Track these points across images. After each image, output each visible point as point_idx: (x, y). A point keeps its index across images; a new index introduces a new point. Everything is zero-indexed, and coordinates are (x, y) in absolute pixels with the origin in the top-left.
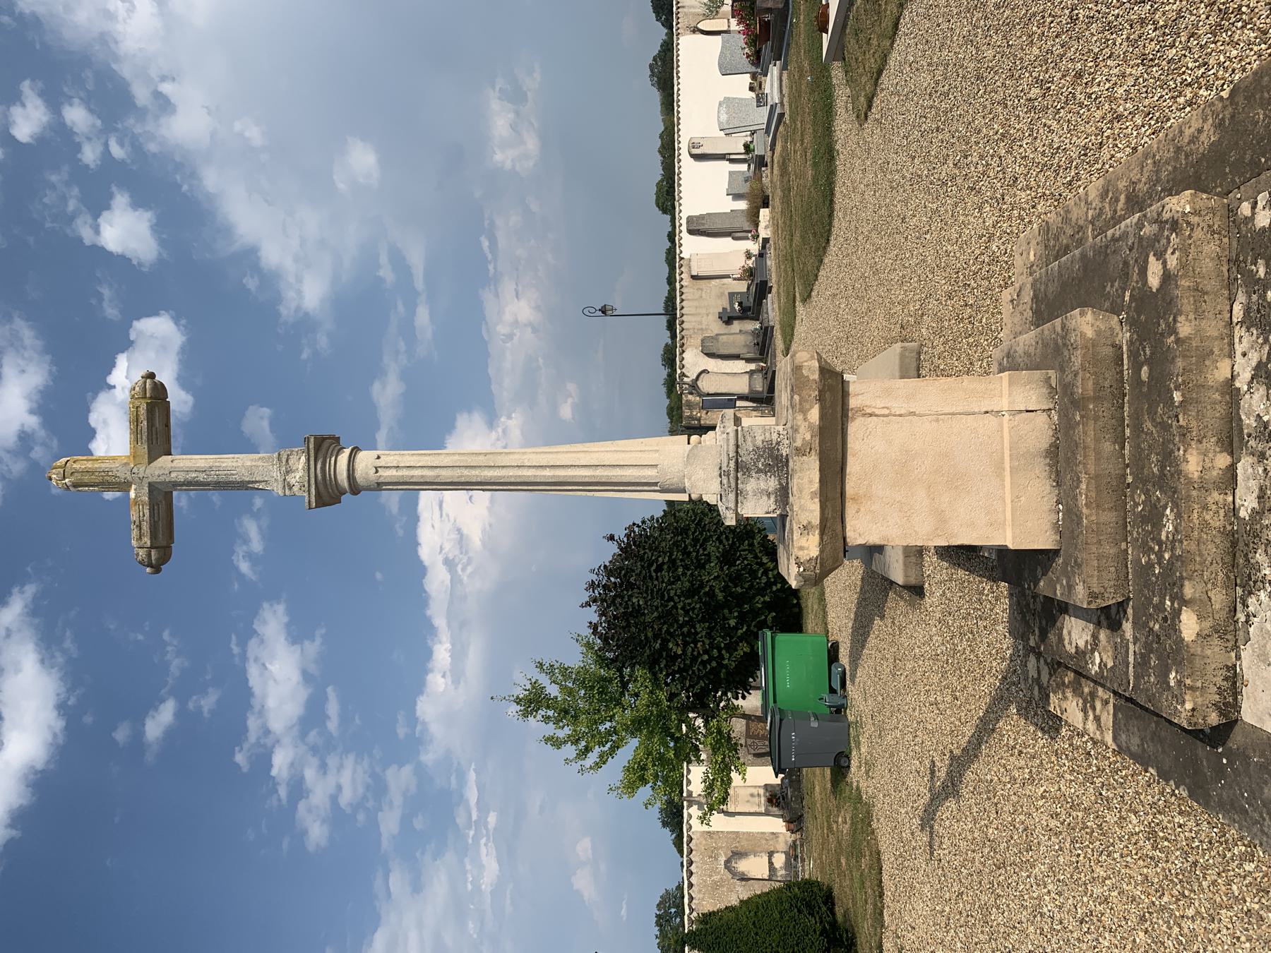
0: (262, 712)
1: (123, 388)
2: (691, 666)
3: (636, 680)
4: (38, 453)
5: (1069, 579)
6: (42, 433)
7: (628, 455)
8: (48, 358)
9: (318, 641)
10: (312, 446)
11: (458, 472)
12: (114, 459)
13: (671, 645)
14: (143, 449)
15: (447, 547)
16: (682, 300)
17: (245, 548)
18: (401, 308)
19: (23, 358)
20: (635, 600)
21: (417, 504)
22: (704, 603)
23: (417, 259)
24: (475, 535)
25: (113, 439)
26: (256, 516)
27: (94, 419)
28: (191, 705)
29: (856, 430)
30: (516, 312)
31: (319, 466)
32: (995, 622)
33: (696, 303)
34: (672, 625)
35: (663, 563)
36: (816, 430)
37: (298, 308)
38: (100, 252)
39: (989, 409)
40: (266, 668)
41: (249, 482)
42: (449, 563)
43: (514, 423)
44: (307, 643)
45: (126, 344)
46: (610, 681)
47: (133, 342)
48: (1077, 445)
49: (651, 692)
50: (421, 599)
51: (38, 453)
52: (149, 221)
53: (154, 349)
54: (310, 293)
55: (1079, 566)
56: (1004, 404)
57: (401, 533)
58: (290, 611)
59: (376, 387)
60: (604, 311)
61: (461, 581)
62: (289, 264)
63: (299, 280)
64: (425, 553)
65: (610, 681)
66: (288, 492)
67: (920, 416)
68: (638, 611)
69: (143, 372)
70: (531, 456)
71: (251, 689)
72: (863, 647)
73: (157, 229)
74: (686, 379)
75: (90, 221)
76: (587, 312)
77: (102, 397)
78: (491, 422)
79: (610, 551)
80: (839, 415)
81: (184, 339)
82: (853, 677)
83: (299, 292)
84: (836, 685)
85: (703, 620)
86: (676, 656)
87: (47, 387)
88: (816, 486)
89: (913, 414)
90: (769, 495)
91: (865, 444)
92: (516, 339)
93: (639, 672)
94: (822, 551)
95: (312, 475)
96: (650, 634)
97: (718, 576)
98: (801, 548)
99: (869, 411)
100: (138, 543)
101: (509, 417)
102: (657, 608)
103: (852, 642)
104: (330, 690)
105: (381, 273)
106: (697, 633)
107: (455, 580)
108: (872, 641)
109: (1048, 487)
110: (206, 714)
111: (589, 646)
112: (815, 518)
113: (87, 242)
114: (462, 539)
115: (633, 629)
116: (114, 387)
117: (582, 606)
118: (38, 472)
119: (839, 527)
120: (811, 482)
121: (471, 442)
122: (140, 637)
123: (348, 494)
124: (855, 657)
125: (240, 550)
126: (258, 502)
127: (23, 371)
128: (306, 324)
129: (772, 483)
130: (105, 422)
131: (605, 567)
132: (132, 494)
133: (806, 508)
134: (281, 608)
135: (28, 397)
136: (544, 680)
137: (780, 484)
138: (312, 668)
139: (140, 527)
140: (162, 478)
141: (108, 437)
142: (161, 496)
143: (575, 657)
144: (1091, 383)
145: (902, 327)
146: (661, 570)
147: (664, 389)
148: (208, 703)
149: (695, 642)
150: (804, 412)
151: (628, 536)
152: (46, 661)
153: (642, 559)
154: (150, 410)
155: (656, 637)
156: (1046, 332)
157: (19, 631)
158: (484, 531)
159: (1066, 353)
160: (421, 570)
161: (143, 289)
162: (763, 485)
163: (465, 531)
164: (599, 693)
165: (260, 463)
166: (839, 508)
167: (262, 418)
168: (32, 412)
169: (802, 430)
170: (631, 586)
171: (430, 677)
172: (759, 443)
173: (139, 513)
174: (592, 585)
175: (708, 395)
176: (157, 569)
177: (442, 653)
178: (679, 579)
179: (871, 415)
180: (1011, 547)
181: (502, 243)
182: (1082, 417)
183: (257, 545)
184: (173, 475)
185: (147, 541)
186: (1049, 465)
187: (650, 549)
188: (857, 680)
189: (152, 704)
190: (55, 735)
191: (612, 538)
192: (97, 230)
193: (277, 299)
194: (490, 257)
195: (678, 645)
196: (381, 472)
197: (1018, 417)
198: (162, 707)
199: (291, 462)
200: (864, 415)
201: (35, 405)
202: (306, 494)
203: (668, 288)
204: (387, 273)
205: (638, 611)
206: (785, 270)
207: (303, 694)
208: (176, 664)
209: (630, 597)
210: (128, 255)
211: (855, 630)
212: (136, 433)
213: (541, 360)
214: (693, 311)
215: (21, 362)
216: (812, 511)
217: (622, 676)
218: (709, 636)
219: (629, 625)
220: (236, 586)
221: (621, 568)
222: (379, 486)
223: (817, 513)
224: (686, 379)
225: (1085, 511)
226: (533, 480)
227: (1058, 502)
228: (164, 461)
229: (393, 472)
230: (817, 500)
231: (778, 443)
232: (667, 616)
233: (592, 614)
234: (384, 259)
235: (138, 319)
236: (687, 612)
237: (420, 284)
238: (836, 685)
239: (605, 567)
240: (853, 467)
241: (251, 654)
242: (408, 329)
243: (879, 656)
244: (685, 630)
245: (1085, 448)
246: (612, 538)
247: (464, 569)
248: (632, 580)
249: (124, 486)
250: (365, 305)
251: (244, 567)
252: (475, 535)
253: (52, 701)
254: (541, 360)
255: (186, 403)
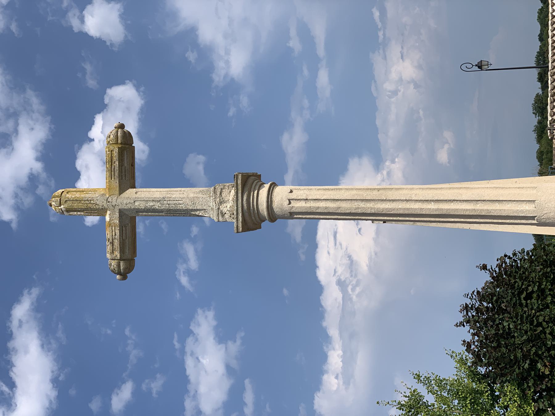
0: (195, 397)
1: (99, 141)
3: (505, 395)
4: (41, 190)
6: (44, 175)
7: (506, 192)
8: (49, 118)
9: (239, 342)
10: (239, 182)
11: (355, 205)
12: (95, 191)
13: (539, 365)
14: (116, 183)
15: (340, 270)
17: (185, 266)
18: (306, 72)
19: (32, 119)
20: (505, 324)
21: (316, 234)
23: (319, 31)
24: (363, 260)
25: (93, 175)
26: (193, 241)
27: (79, 164)
28: (144, 387)
30: (401, 71)
31: (245, 198)
34: (540, 348)
35: (533, 292)
37: (226, 75)
38: (84, 36)
40: (199, 361)
41: (192, 210)
42: (341, 284)
43: (397, 167)
44: (230, 343)
45: (101, 107)
46: (482, 393)
47: (106, 105)
49: (519, 406)
50: (318, 312)
51: (41, 190)
52: (119, 10)
53: (123, 106)
54: (235, 62)
57: (303, 257)
58: (217, 317)
59: (285, 137)
60: (480, 66)
61: (351, 299)
62: (220, 40)
63: (228, 52)
64: (322, 274)
65: (482, 393)
66: (221, 219)
68: (508, 334)
69: (116, 124)
70: (417, 192)
71: (187, 377)
73: (123, 17)
75: (78, 14)
76: (465, 68)
77: (85, 147)
78: (378, 165)
79: (483, 279)
81: (143, 102)
83: (227, 62)
86: (544, 376)
87: (47, 140)
92: (400, 94)
93: (508, 388)
95: (240, 206)
96: (519, 355)
100: (112, 256)
101: (393, 162)
104: (247, 382)
105: (291, 44)
107: (346, 297)
110: (154, 395)
111: (462, 362)
113: (76, 30)
114: (352, 264)
115: (504, 350)
116: (93, 140)
117: (457, 325)
118: (42, 205)
121: (360, 182)
122: (109, 332)
123: (267, 222)
125: (182, 268)
126: (195, 230)
127: (32, 129)
128: (232, 87)
130: (87, 167)
131: (478, 292)
132: (107, 218)
134: (211, 314)
135: (35, 148)
136: (422, 390)
138: (234, 364)
139: (112, 243)
140: (129, 206)
141: (89, 178)
142: (128, 220)
143: (450, 371)
146: (531, 298)
147: (534, 135)
148: (156, 385)
151: (499, 266)
152: (44, 346)
153: (513, 287)
154: (121, 152)
157: (28, 322)
158: (370, 259)
160: (318, 288)
161: (113, 63)
163: (355, 258)
164: (471, 403)
165: (200, 195)
167: (198, 163)
168: (38, 159)
170: (502, 311)
171: (325, 377)
173: (112, 233)
174: (466, 308)
176: (124, 277)
177: (335, 358)
178: (548, 307)
181: (390, 13)
183: (193, 264)
184: (137, 204)
185: (117, 254)
187: (521, 278)
189: (114, 385)
190: (51, 402)
191: (484, 267)
192: (82, 20)
193: (211, 68)
194: (380, 25)
195: (545, 366)
196: (293, 204)
198: (123, 386)
199: (223, 195)
201: (39, 154)
202: (234, 221)
203: (539, 44)
204: (295, 44)
205: (509, 334)
207: (227, 384)
208: (134, 354)
209: (502, 320)
210: (104, 38)
212: (111, 171)
213: (421, 112)
215: (31, 122)
217: (493, 391)
219: (499, 346)
220: (178, 295)
221: (493, 295)
222: (292, 215)
226: (419, 212)
228: (130, 193)
229: (302, 204)
232: (536, 339)
233: (466, 334)
234: (293, 32)
235: (110, 87)
237: (321, 51)
239: (478, 292)
241: (188, 349)
242: (311, 89)
246: (484, 267)
247: (353, 290)
248: (503, 306)
249: (101, 212)
250: (278, 68)
251: (184, 280)
252: (363, 260)
253: (48, 376)
254: (421, 112)
255: (143, 152)
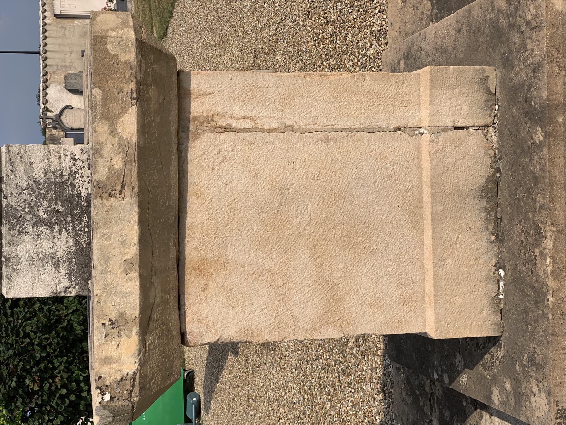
2: (49, 401)
5: (517, 383)
13: (27, 381)
16: (45, 38)
22: (63, 338)
29: (201, 152)
32: (362, 380)
33: (58, 41)
36: (133, 152)
39: (402, 124)
48: (536, 180)
55: (540, 367)
56: (423, 116)
67: (302, 132)
72: (217, 380)
74: (49, 114)
80: (174, 127)
82: (207, 408)
84: (191, 415)
85: (61, 355)
86: (34, 393)
88: (133, 250)
89: (289, 129)
90: (57, 264)
91: (215, 175)
94: (142, 364)
97: (77, 310)
98: (107, 361)
99: (222, 122)
102: (12, 345)
103: (207, 373)
106: (54, 369)
108: (225, 376)
109: (484, 243)
112: (133, 308)
119: (174, 317)
120: (124, 243)
124: (210, 389)
129: (63, 243)
133: (117, 292)
137: (77, 244)
144: (560, 82)
145: (256, 56)
149: (53, 377)
150: (111, 119)
155: (11, 374)
156: (476, 12)
159: (516, 38)
162: (46, 246)
166: (173, 285)
169: (107, 150)
172: (38, 174)
175: (72, 130)
178: (35, 315)
179: (225, 129)
180: (433, 335)
182: (547, 135)
186: (486, 210)
188: (211, 412)
197: (443, 137)
200: (214, 129)
206: (143, 10)
211: (209, 363)
214: (57, 48)
216: (126, 295)
218: (68, 370)
223: (135, 298)
224: (49, 114)
225: (551, 283)
227: (498, 266)
230: (135, 275)
231: (73, 175)
236: (43, 348)
238: (191, 415)
240: (197, 215)
243: (232, 392)
244: (42, 366)
245: (551, 184)
